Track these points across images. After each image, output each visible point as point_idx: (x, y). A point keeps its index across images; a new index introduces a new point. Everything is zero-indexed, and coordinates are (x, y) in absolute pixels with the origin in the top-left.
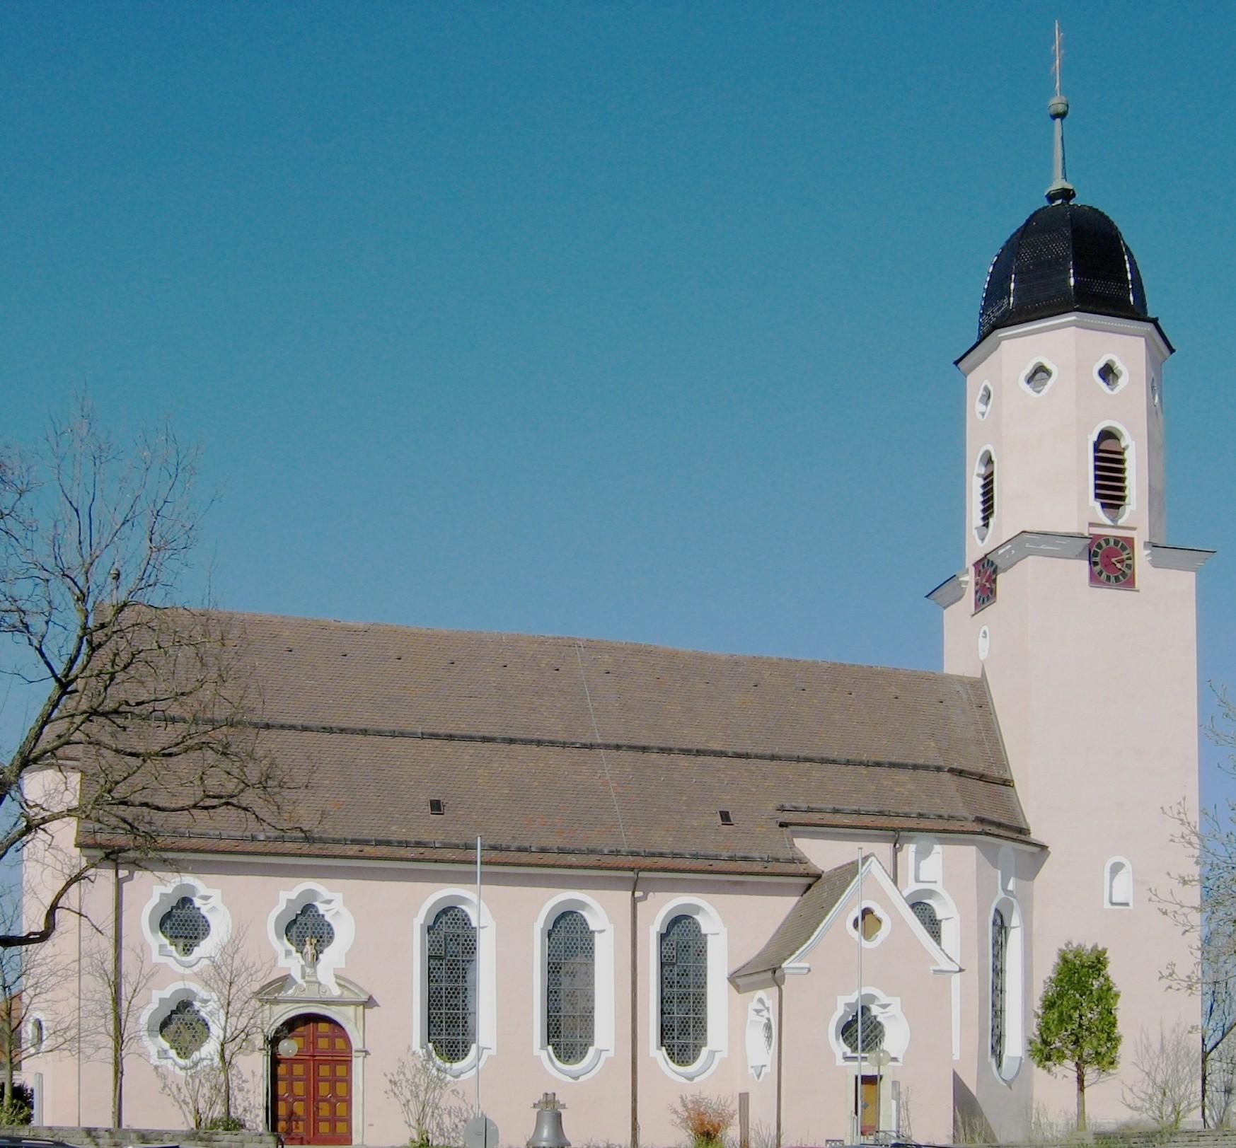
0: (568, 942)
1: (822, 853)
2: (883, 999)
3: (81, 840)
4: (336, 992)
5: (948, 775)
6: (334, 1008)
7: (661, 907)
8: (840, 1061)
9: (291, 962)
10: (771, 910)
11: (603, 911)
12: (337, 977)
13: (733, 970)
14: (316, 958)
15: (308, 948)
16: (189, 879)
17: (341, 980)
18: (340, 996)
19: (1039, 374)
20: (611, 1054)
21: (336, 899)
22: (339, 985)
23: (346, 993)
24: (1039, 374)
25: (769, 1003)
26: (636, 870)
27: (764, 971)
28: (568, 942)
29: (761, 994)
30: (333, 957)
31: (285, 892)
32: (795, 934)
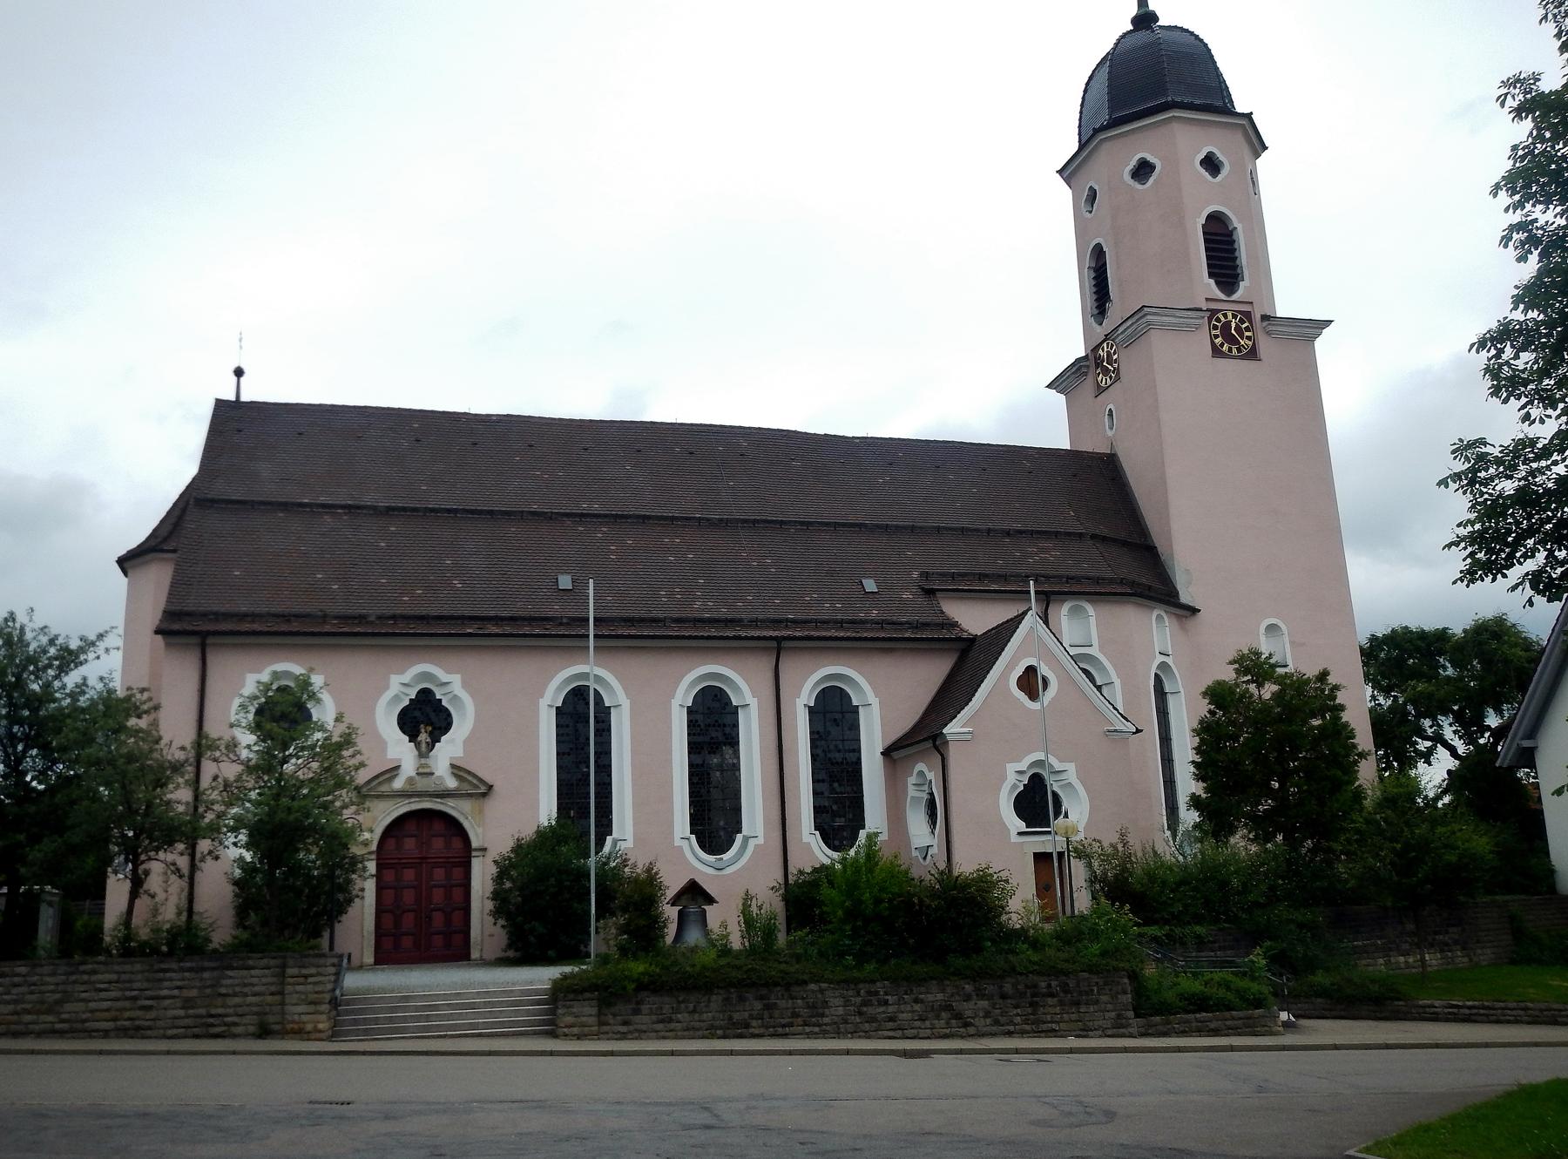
0: (712, 725)
1: (974, 618)
2: (1057, 766)
3: (165, 626)
4: (452, 783)
5: (1090, 542)
6: (451, 802)
7: (806, 681)
8: (1014, 838)
9: (400, 750)
10: (920, 678)
11: (745, 686)
12: (453, 766)
13: (889, 742)
14: (431, 746)
15: (423, 737)
16: (291, 666)
17: (456, 770)
18: (457, 789)
19: (1143, 170)
20: (761, 841)
21: (453, 679)
22: (455, 775)
23: (466, 786)
24: (1143, 170)
25: (930, 776)
26: (779, 640)
27: (923, 738)
28: (712, 725)
29: (921, 766)
30: (448, 750)
31: (400, 681)
32: (951, 697)
